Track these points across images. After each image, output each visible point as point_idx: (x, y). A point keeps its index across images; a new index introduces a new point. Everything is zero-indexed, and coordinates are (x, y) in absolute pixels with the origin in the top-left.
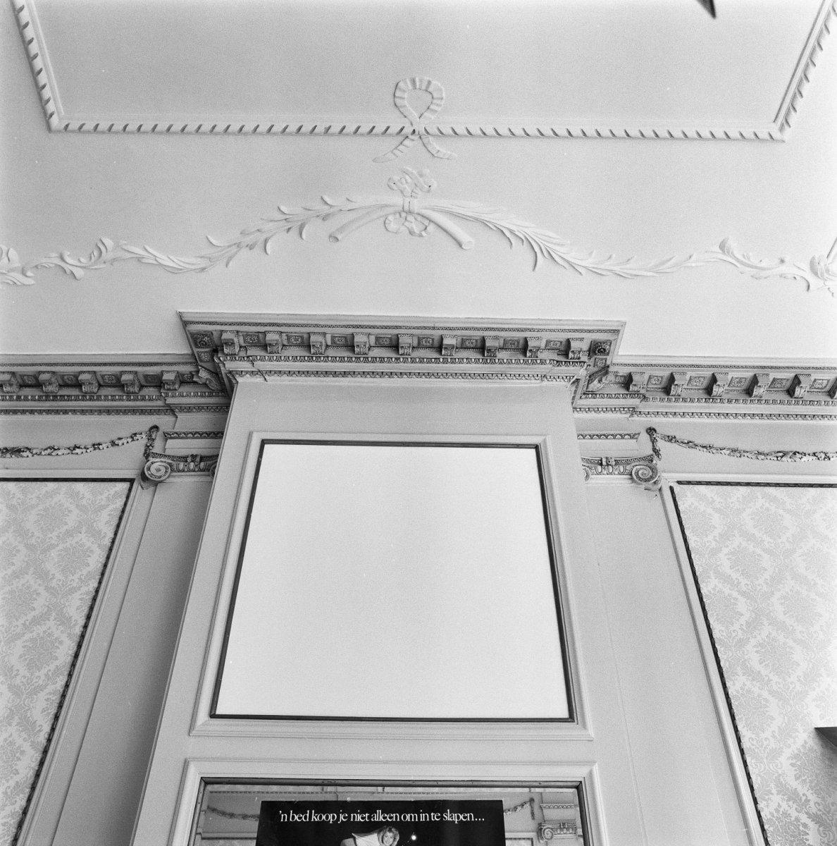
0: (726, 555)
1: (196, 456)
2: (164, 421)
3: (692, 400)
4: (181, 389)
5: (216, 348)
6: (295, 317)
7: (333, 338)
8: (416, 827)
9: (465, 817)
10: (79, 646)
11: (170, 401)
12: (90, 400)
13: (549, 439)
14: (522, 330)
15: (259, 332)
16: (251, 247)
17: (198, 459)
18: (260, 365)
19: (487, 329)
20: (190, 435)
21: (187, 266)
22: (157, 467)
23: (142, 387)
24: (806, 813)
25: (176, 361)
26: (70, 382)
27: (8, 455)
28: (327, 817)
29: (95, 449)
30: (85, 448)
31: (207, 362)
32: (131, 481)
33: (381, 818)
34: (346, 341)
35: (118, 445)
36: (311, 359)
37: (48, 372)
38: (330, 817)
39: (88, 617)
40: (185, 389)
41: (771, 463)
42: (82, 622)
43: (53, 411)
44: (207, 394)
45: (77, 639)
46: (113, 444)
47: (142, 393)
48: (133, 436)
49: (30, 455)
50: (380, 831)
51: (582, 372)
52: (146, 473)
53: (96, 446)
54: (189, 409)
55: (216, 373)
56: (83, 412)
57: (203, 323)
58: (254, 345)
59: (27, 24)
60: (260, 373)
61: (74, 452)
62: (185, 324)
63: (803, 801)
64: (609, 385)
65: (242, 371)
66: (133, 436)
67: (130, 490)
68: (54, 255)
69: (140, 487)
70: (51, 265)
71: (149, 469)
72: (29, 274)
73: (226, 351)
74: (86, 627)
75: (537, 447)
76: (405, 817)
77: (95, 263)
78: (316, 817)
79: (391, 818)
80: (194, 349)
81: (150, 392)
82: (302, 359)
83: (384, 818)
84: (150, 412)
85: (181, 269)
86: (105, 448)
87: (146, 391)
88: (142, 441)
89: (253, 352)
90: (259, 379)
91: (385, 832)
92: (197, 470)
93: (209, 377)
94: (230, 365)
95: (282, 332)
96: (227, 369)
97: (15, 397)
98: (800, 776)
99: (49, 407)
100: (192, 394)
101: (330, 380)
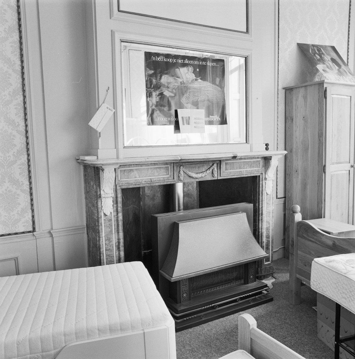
0: (15, 105)
9: (213, 64)
24: (16, 130)
28: (169, 60)
33: (187, 62)
38: (170, 60)
50: (187, 67)
63: (21, 184)
76: (195, 63)
78: (165, 59)
79: (190, 62)
83: (189, 62)
91: (189, 68)
98: (22, 173)
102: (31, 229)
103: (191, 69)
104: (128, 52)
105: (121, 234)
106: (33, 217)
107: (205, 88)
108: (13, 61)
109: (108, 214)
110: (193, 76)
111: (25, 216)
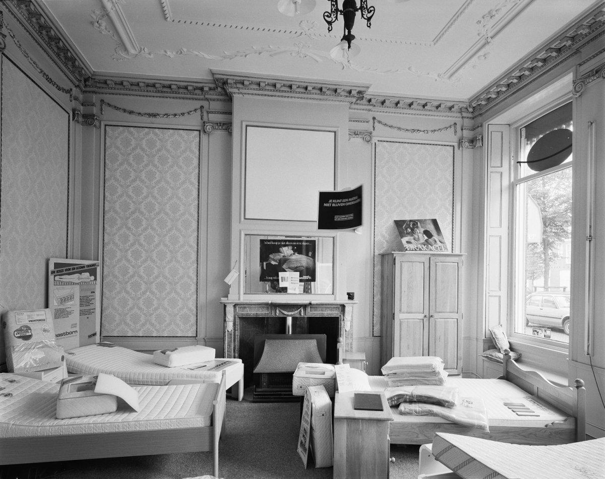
3: (390, 107)
5: (225, 83)
8: (296, 245)
11: (207, 96)
13: (339, 130)
14: (335, 85)
19: (323, 84)
32: (200, 131)
41: (409, 134)
48: (195, 110)
51: (354, 100)
53: (183, 114)
62: (213, 74)
64: (364, 101)
66: (195, 110)
75: (335, 132)
81: (198, 92)
82: (257, 89)
89: (239, 85)
90: (241, 95)
94: (231, 90)
101: (266, 98)
102: (195, 336)
103: (290, 248)
104: (450, 144)
105: (237, 343)
106: (197, 328)
107: (303, 260)
109: (230, 331)
110: (292, 252)
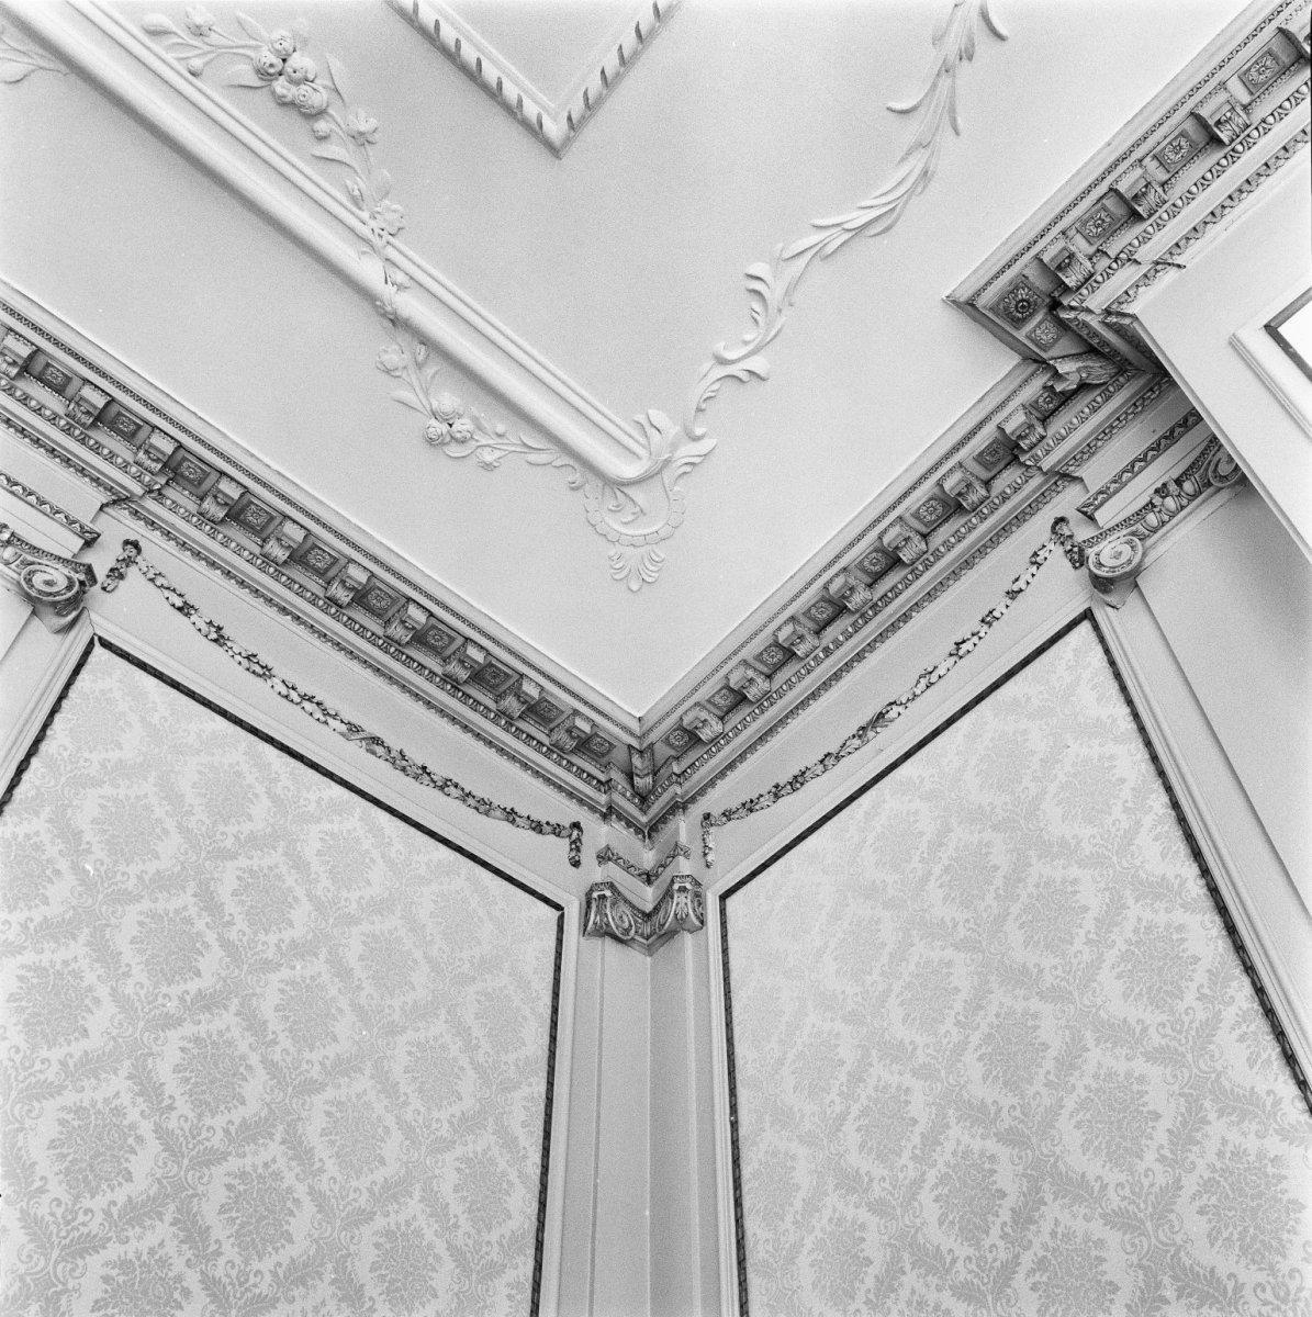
1: (1164, 485)
2: (1067, 501)
4: (1051, 431)
6: (1140, 118)
7: (1244, 78)
10: (1222, 910)
11: (1046, 464)
12: (926, 568)
15: (1098, 201)
16: (967, 55)
17: (1173, 487)
18: (1147, 253)
20: (1126, 476)
21: (898, 193)
22: (1111, 554)
23: (987, 484)
25: (1012, 387)
26: (878, 568)
27: (871, 734)
29: (990, 624)
30: (973, 635)
31: (1056, 341)
32: (1087, 615)
34: (1276, 59)
35: (1021, 590)
36: (1233, 156)
37: (837, 575)
39: (1197, 854)
40: (1057, 425)
42: (1192, 870)
43: (887, 630)
44: (1099, 399)
45: (1208, 903)
46: (1013, 594)
47: (994, 493)
49: (901, 709)
52: (1104, 574)
53: (989, 619)
54: (1089, 450)
55: (1091, 348)
56: (930, 596)
57: (996, 277)
58: (1111, 231)
59: (437, 23)
60: (1160, 264)
61: (961, 653)
65: (1126, 292)
67: (1096, 627)
68: (707, 365)
69: (1109, 609)
70: (715, 387)
71: (1100, 565)
72: (699, 431)
73: (1071, 281)
74: (1205, 872)
77: (769, 325)
80: (1021, 335)
84: (1032, 508)
85: (893, 210)
86: (1004, 611)
87: (999, 485)
88: (1057, 557)
92: (1185, 502)
93: (1080, 364)
94: (1097, 300)
95: (1140, 161)
96: (1098, 311)
97: (821, 655)
98: (21, 1000)
99: (878, 627)
100: (1075, 421)
108: (316, 873)
111: (1231, 997)
